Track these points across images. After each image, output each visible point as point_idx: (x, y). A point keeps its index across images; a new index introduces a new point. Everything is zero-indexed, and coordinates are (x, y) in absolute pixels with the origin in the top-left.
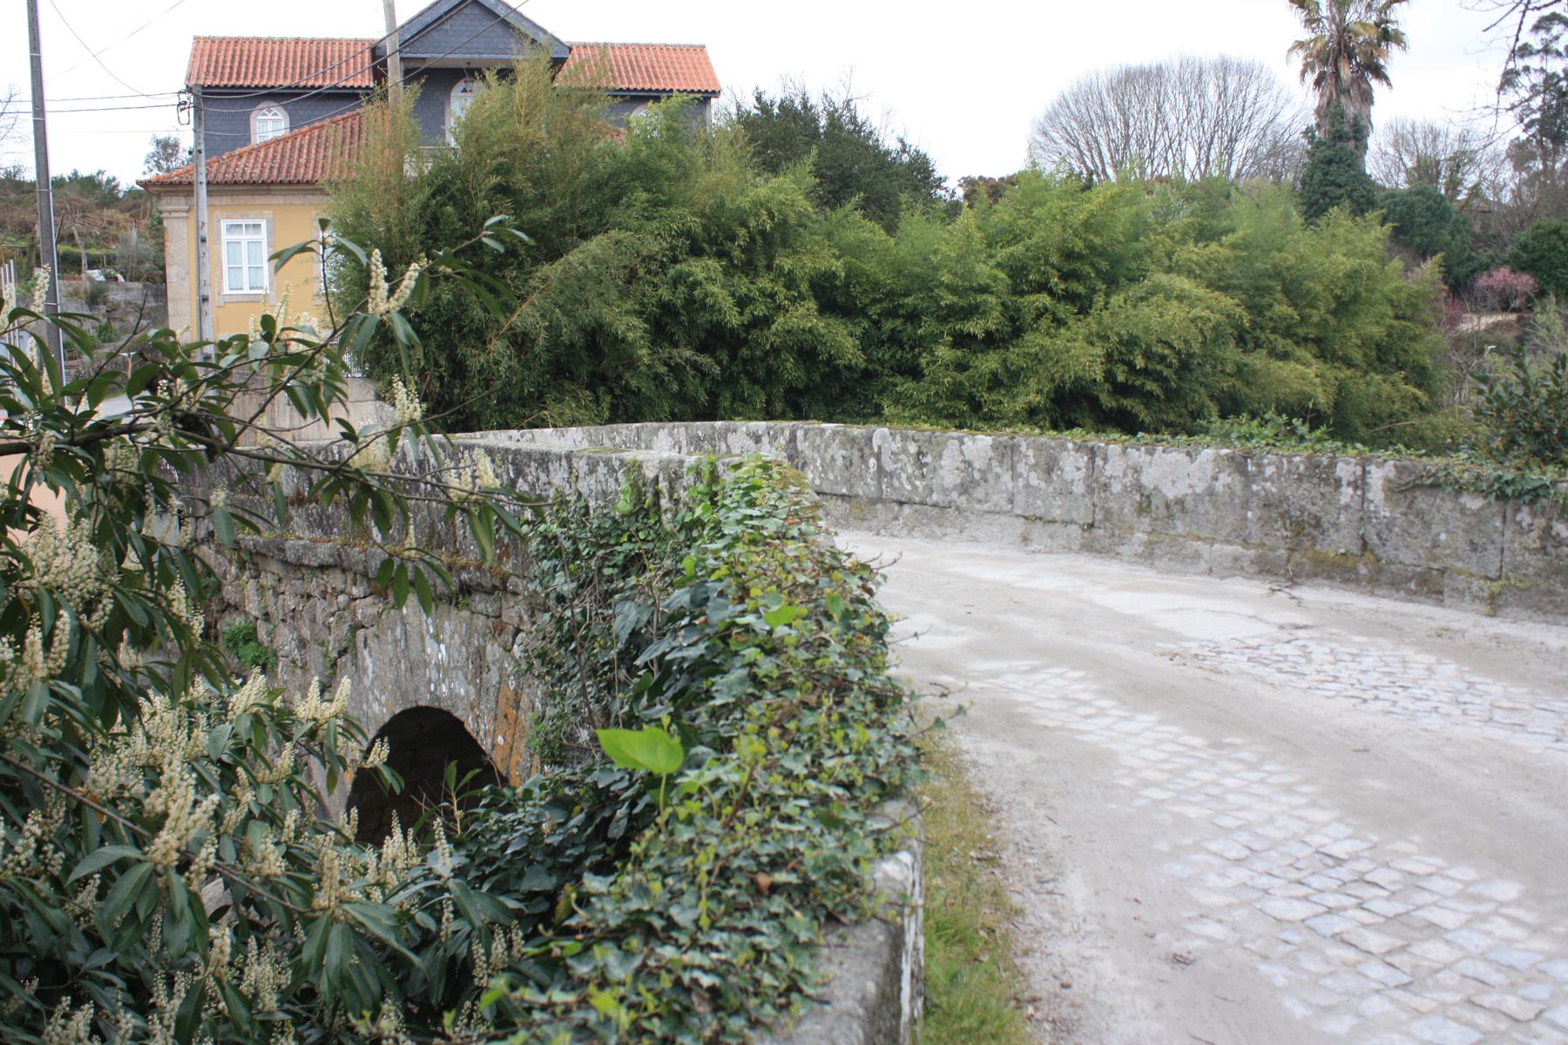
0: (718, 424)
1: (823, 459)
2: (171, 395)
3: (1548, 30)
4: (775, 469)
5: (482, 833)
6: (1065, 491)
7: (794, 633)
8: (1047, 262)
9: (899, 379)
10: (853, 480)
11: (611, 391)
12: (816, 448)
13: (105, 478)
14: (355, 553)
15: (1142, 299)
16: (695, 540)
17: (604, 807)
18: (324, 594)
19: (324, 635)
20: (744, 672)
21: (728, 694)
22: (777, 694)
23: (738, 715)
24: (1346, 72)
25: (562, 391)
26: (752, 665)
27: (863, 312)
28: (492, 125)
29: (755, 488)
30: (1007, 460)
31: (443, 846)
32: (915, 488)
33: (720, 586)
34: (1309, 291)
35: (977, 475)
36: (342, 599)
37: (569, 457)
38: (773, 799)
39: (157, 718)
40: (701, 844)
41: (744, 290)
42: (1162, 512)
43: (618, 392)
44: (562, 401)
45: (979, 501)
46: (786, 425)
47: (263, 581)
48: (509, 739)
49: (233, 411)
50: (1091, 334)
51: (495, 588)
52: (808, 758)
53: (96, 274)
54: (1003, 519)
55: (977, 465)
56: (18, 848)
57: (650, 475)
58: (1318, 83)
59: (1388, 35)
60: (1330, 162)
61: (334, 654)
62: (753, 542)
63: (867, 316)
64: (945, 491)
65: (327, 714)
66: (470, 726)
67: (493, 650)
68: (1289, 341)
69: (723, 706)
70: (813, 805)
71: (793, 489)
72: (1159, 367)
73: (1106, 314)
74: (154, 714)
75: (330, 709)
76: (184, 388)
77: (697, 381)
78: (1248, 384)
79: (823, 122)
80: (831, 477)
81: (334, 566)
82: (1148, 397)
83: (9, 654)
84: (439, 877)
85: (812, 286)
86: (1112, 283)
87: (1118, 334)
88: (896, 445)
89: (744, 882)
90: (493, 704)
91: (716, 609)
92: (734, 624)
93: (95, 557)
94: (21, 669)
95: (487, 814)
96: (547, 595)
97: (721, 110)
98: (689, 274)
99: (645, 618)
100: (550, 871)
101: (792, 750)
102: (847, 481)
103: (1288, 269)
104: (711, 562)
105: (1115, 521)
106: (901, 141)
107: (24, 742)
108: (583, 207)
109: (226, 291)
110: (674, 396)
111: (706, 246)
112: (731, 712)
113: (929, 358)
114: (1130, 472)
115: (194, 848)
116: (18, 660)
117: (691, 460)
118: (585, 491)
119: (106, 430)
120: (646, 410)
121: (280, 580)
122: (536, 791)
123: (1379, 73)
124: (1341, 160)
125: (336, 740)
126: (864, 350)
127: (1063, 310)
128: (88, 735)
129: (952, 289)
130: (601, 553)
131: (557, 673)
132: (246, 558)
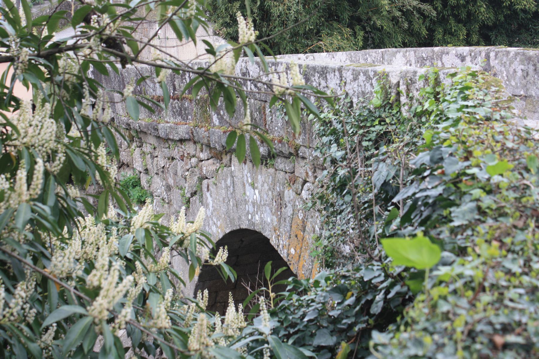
0: (436, 49)
1: (508, 72)
2: (99, 25)
4: (481, 76)
5: (287, 308)
7: (505, 180)
10: (529, 86)
11: (364, 28)
12: (504, 64)
13: (58, 78)
14: (202, 132)
16: (424, 124)
17: (367, 294)
18: (182, 158)
19: (182, 183)
20: (473, 205)
21: (463, 218)
22: (496, 219)
23: (469, 232)
26: (478, 200)
29: (468, 88)
31: (265, 314)
33: (450, 150)
36: (194, 160)
37: (340, 70)
38: (498, 288)
39: (87, 230)
40: (455, 314)
43: (368, 29)
44: (331, 35)
46: (483, 49)
47: (144, 149)
48: (298, 251)
49: (136, 36)
51: (291, 154)
52: (521, 262)
56: (12, 305)
57: (394, 81)
61: (189, 195)
62: (470, 122)
65: (190, 230)
66: (273, 242)
67: (289, 194)
69: (459, 227)
70: (527, 293)
71: (493, 89)
74: (85, 227)
75: (191, 228)
76: (108, 21)
77: (421, 21)
80: (513, 83)
81: (190, 140)
83: (7, 185)
84: (261, 334)
89: (485, 341)
90: (288, 228)
91: (451, 164)
92: (465, 174)
93: (54, 127)
94: (14, 195)
95: (290, 295)
96: (325, 159)
99: (393, 173)
100: (332, 333)
101: (510, 256)
102: (525, 86)
104: (443, 135)
107: (14, 240)
110: (405, 31)
112: (464, 230)
115: (117, 309)
116: (12, 189)
117: (422, 71)
118: (351, 92)
119: (59, 47)
120: (386, 40)
121: (155, 148)
122: (323, 282)
125: (195, 247)
128: (48, 238)
130: (361, 131)
131: (331, 209)
132: (134, 134)
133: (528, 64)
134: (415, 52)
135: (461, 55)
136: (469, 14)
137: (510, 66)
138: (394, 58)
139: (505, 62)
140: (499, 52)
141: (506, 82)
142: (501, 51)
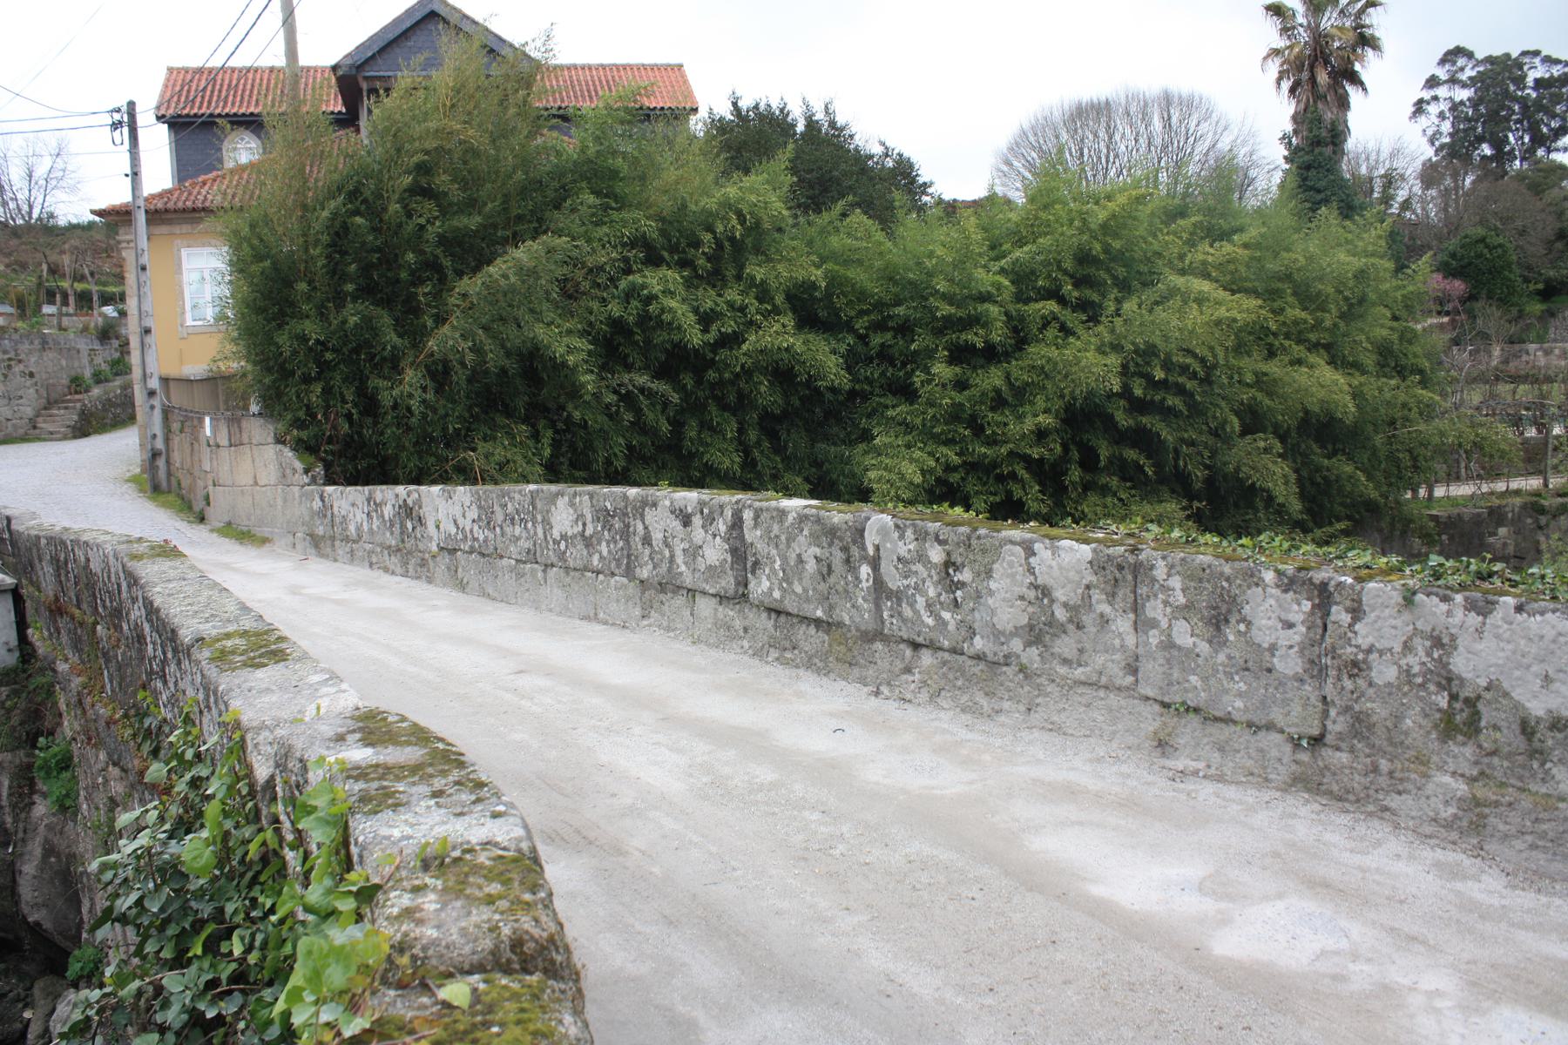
0: (633, 492)
1: (784, 559)
3: (1454, 63)
6: (1257, 665)
8: (1059, 268)
9: (889, 400)
10: (834, 599)
11: (553, 424)
12: (774, 541)
15: (1157, 303)
24: (1323, 77)
25: (494, 427)
27: (849, 327)
28: (414, 118)
30: (1124, 592)
32: (943, 623)
34: (1319, 293)
35: (1061, 614)
41: (709, 304)
42: (1509, 737)
43: (560, 425)
45: (1066, 661)
50: (1103, 344)
53: (109, 310)
54: (1114, 699)
55: (1060, 594)
58: (1292, 91)
59: (1366, 41)
60: (1308, 167)
63: (852, 330)
64: (997, 635)
68: (1302, 348)
72: (1180, 380)
73: (1118, 321)
78: (1270, 394)
79: (800, 128)
80: (799, 590)
82: (1167, 413)
85: (790, 297)
86: (1125, 287)
87: (1133, 343)
88: (906, 547)
97: (697, 125)
98: (644, 286)
103: (1299, 270)
105: (1379, 740)
106: (882, 144)
108: (515, 212)
109: (189, 322)
111: (666, 254)
113: (923, 376)
114: (1420, 645)
123: (1355, 79)
124: (1320, 166)
126: (849, 369)
127: (1071, 318)
129: (948, 298)
133: (831, 545)
134: (592, 497)
135: (681, 510)
136: (741, 396)
137: (788, 546)
138: (553, 509)
139: (777, 537)
140: (761, 509)
141: (781, 584)
142: (767, 509)
